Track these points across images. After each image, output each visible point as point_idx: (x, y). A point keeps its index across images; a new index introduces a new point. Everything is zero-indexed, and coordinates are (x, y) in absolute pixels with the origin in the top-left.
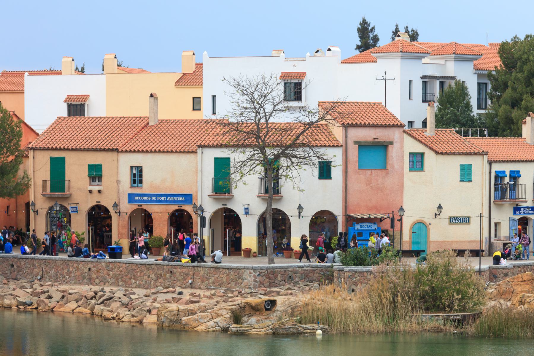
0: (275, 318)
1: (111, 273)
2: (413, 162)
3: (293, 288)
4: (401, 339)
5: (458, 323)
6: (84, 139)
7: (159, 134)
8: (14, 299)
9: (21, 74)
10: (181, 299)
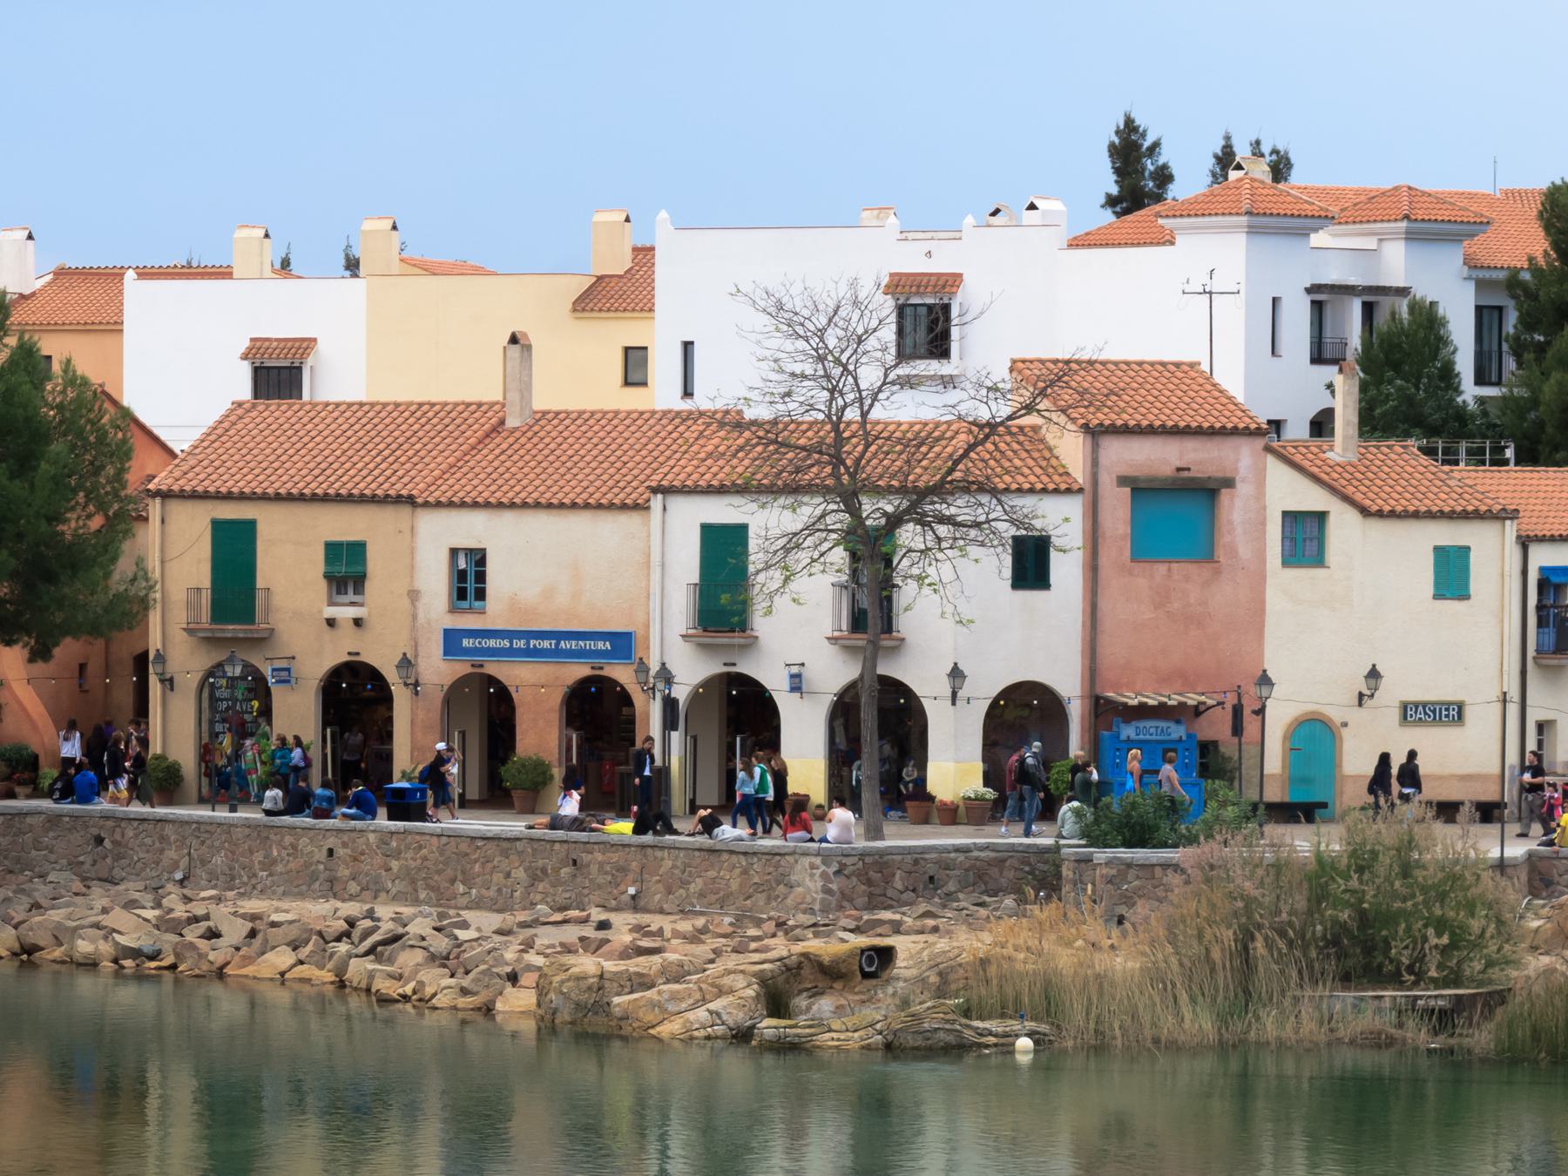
0: (889, 1000)
1: (395, 864)
2: (1293, 540)
3: (939, 912)
4: (1268, 1065)
5: (1440, 1019)
6: (311, 465)
7: (534, 452)
8: (106, 938)
9: (114, 276)
10: (608, 941)
